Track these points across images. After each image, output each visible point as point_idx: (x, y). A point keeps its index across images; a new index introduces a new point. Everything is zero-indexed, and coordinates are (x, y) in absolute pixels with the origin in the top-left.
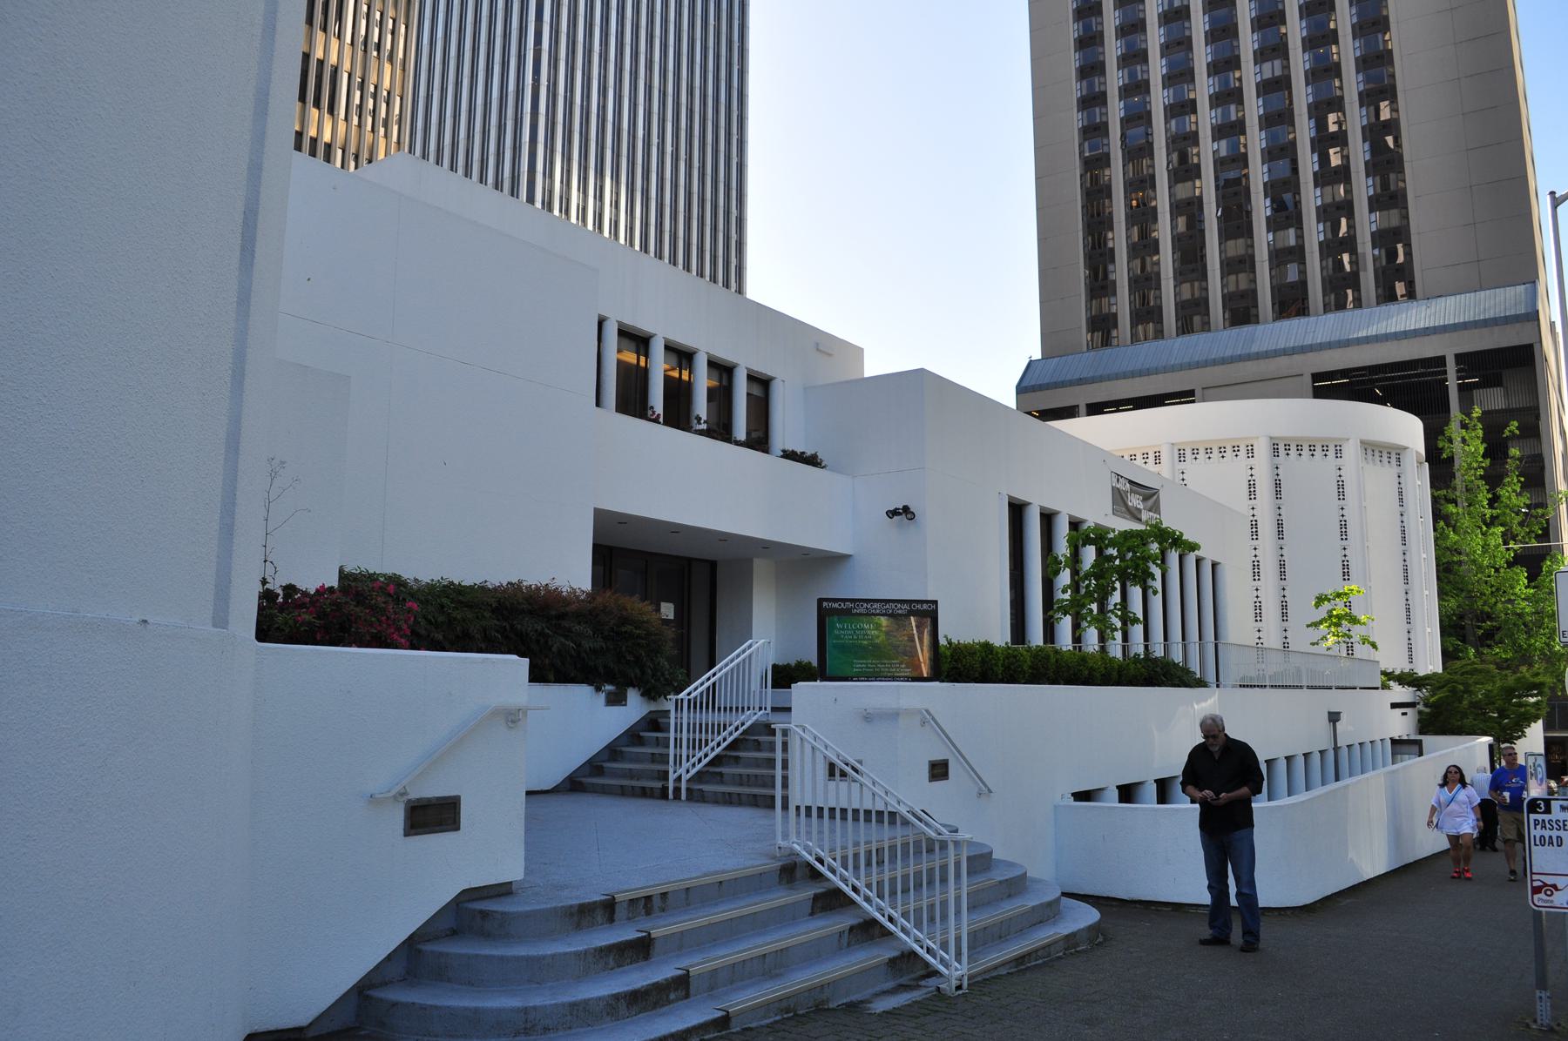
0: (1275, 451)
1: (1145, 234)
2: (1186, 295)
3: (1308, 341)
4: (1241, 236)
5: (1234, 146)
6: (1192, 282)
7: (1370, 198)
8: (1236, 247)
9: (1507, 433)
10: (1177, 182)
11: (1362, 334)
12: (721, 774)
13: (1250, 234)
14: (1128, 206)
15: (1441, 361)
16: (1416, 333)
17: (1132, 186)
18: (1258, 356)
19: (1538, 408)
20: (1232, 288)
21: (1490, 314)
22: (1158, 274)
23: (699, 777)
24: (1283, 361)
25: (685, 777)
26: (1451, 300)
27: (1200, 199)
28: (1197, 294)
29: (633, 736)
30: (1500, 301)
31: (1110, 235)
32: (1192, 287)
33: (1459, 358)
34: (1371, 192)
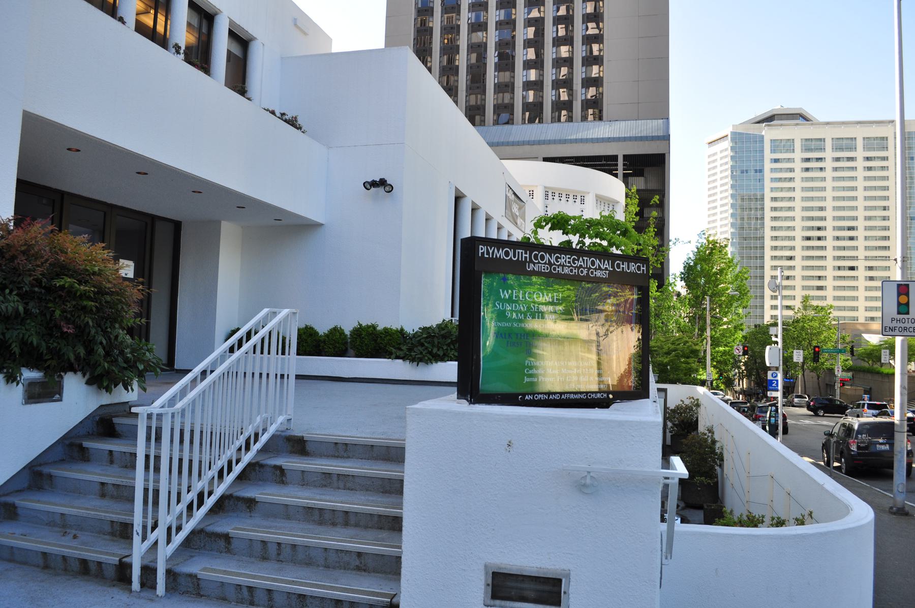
0: (547, 195)
1: (451, 61)
2: (473, 102)
3: (542, 138)
4: (507, 70)
5: (509, 15)
6: (476, 94)
7: (583, 58)
8: (505, 76)
9: (652, 202)
10: (473, 31)
11: (574, 137)
12: (227, 538)
13: (513, 70)
14: (442, 42)
15: (615, 158)
16: (609, 140)
17: (445, 30)
18: (514, 144)
19: (664, 190)
20: (500, 101)
21: (644, 134)
22: (457, 87)
23: (197, 541)
24: (527, 148)
25: (165, 552)
26: (623, 124)
27: (486, 44)
28: (479, 103)
29: (72, 448)
30: (649, 127)
31: (429, 59)
32: (477, 98)
33: (624, 156)
34: (584, 54)
